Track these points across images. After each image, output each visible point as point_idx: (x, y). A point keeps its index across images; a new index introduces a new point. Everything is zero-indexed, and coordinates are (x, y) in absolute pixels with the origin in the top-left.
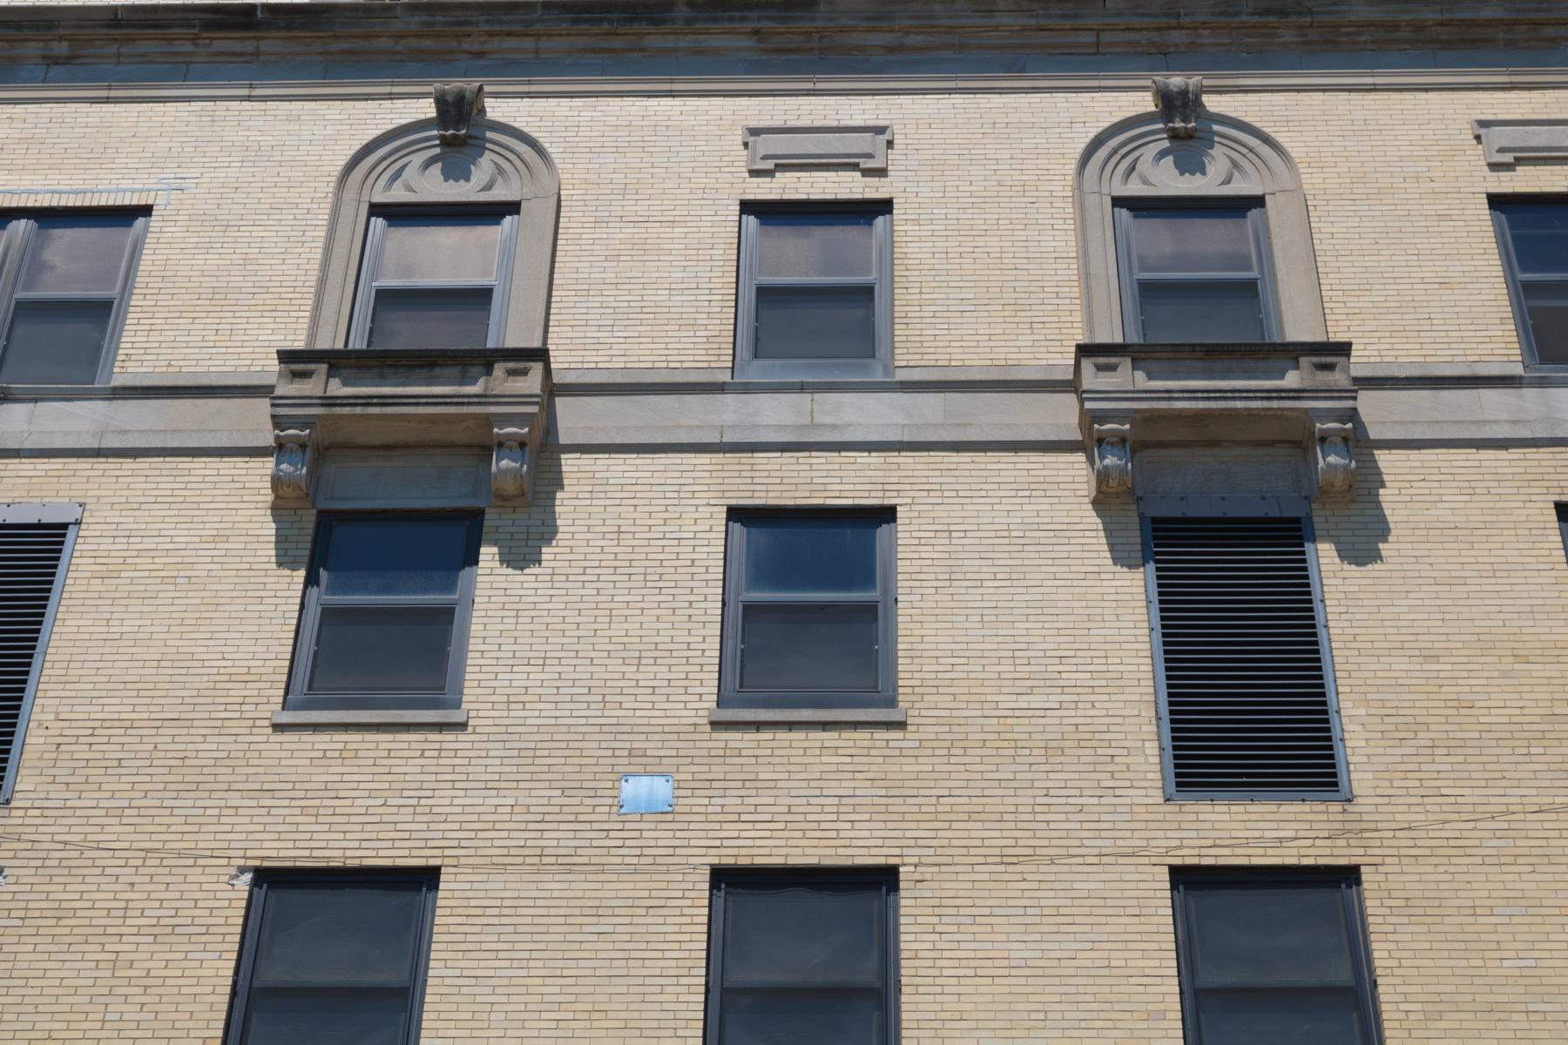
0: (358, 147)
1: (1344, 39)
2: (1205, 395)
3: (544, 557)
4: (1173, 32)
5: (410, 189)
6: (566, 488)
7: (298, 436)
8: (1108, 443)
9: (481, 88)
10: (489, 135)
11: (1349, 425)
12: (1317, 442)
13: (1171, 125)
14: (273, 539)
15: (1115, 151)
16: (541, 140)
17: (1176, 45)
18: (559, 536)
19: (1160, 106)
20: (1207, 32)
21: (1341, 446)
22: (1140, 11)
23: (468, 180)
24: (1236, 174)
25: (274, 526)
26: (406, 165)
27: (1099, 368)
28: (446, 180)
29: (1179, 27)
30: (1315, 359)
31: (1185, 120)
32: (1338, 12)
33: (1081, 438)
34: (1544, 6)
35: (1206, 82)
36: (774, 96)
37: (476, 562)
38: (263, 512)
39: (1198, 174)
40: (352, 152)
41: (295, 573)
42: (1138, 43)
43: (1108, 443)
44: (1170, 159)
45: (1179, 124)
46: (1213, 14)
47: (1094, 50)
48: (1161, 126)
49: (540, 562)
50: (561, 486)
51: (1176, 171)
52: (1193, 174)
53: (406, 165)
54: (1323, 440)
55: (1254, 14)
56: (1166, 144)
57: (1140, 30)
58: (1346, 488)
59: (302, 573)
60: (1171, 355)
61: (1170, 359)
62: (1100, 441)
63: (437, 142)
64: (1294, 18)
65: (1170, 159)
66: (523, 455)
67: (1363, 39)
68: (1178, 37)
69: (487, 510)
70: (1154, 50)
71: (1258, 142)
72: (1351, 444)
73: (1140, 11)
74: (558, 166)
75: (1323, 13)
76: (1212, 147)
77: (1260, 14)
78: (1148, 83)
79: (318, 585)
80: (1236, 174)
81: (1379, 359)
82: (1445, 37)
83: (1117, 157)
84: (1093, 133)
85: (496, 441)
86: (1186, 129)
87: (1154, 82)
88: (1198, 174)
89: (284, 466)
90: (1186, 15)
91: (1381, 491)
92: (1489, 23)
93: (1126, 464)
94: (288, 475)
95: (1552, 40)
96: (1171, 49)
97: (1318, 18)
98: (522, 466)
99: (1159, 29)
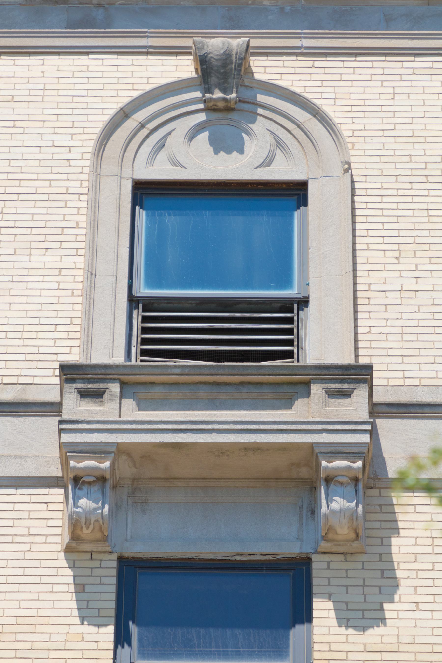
0: (112, 112)
3: (388, 615)
5: (176, 163)
6: (402, 532)
7: (349, 468)
8: (84, 483)
9: (248, 42)
10: (261, 98)
11: (359, 464)
12: (323, 483)
13: (208, 95)
14: (72, 588)
15: (142, 126)
16: (325, 108)
18: (401, 590)
19: (200, 73)
21: (350, 489)
23: (241, 151)
24: (279, 155)
25: (70, 572)
26: (170, 133)
27: (331, 394)
28: (216, 152)
30: (80, 386)
31: (224, 91)
33: (60, 475)
35: (254, 43)
36: (59, 54)
37: (309, 619)
38: (55, 556)
39: (235, 153)
40: (106, 118)
41: (103, 630)
44: (204, 136)
45: (218, 94)
48: (198, 94)
49: (383, 620)
50: (397, 530)
51: (211, 149)
52: (229, 152)
53: (170, 133)
54: (328, 480)
56: (202, 117)
58: (353, 536)
59: (111, 629)
62: (76, 480)
63: (201, 106)
65: (204, 136)
66: (103, 494)
69: (314, 558)
71: (308, 116)
72: (361, 485)
74: (348, 140)
76: (253, 121)
78: (188, 42)
79: (130, 645)
80: (279, 155)
81: (401, 382)
83: (145, 132)
84: (123, 101)
85: (323, 475)
86: (225, 100)
87: (194, 43)
88: (235, 153)
89: (83, 502)
91: (394, 541)
93: (357, 506)
94: (88, 513)
98: (357, 506)
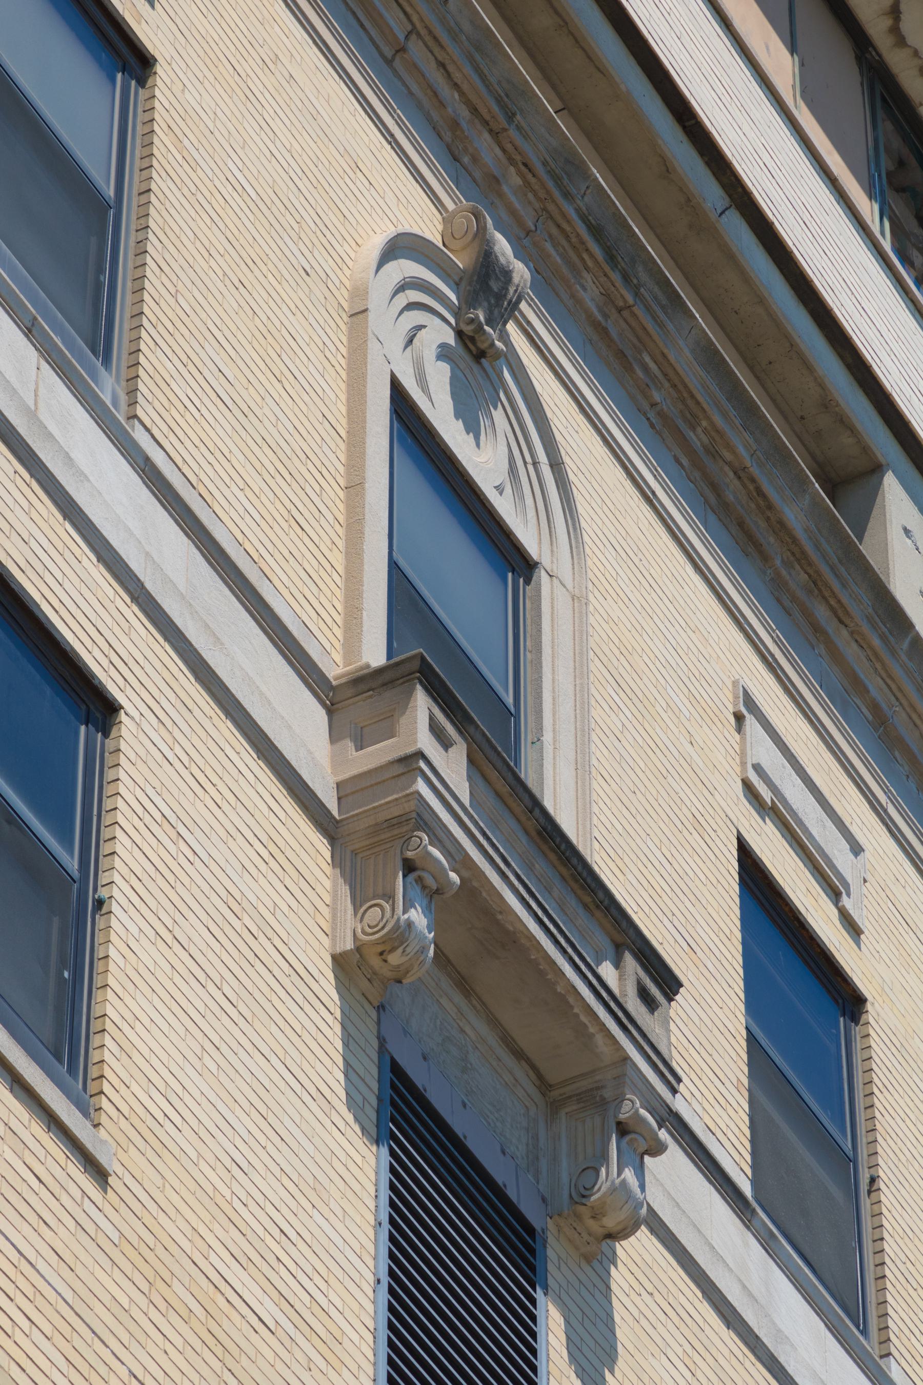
1: (640, 373)
2: (540, 913)
4: (486, 135)
8: (419, 880)
17: (475, 159)
20: (518, 181)
22: (478, 57)
29: (495, 135)
32: (661, 325)
34: (842, 569)
42: (442, 105)
43: (419, 880)
46: (545, 163)
47: (388, 52)
54: (623, 1130)
55: (584, 219)
57: (456, 86)
60: (505, 790)
61: (498, 795)
64: (616, 277)
67: (657, 396)
68: (484, 144)
70: (448, 136)
73: (478, 57)
75: (648, 308)
77: (590, 227)
82: (731, 498)
90: (519, 128)
92: (781, 528)
95: (817, 629)
96: (466, 160)
97: (639, 311)
99: (474, 110)
